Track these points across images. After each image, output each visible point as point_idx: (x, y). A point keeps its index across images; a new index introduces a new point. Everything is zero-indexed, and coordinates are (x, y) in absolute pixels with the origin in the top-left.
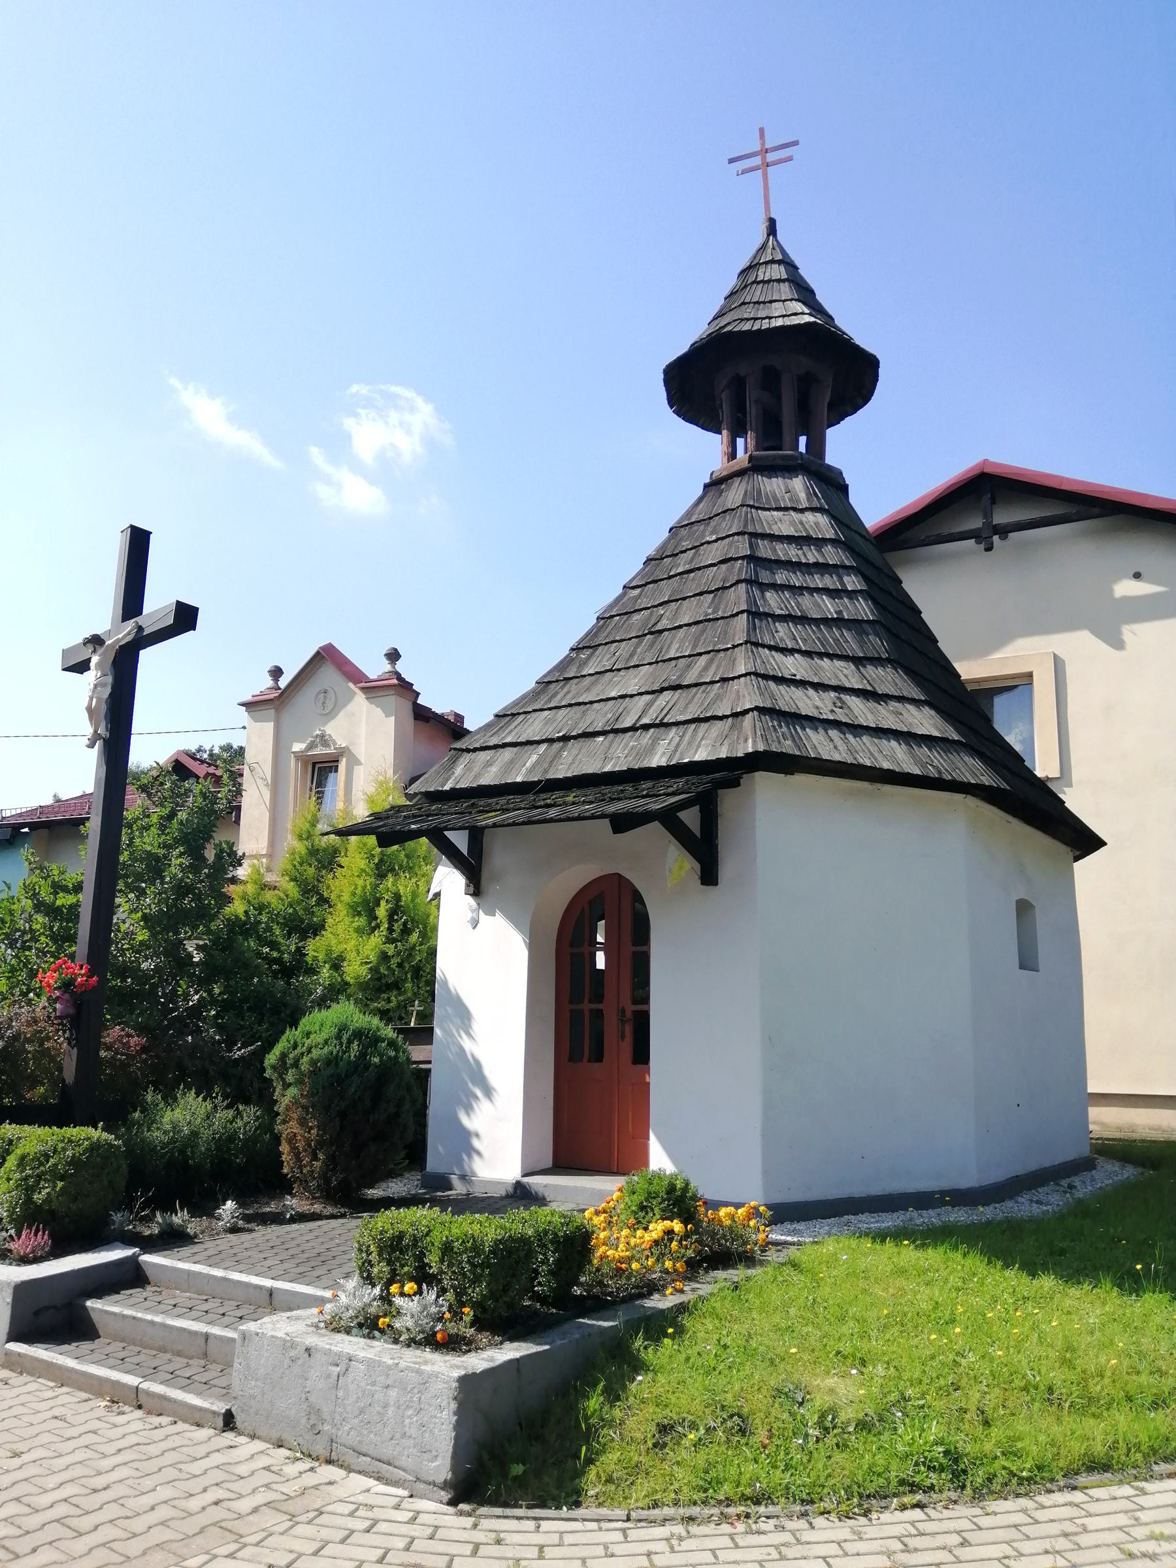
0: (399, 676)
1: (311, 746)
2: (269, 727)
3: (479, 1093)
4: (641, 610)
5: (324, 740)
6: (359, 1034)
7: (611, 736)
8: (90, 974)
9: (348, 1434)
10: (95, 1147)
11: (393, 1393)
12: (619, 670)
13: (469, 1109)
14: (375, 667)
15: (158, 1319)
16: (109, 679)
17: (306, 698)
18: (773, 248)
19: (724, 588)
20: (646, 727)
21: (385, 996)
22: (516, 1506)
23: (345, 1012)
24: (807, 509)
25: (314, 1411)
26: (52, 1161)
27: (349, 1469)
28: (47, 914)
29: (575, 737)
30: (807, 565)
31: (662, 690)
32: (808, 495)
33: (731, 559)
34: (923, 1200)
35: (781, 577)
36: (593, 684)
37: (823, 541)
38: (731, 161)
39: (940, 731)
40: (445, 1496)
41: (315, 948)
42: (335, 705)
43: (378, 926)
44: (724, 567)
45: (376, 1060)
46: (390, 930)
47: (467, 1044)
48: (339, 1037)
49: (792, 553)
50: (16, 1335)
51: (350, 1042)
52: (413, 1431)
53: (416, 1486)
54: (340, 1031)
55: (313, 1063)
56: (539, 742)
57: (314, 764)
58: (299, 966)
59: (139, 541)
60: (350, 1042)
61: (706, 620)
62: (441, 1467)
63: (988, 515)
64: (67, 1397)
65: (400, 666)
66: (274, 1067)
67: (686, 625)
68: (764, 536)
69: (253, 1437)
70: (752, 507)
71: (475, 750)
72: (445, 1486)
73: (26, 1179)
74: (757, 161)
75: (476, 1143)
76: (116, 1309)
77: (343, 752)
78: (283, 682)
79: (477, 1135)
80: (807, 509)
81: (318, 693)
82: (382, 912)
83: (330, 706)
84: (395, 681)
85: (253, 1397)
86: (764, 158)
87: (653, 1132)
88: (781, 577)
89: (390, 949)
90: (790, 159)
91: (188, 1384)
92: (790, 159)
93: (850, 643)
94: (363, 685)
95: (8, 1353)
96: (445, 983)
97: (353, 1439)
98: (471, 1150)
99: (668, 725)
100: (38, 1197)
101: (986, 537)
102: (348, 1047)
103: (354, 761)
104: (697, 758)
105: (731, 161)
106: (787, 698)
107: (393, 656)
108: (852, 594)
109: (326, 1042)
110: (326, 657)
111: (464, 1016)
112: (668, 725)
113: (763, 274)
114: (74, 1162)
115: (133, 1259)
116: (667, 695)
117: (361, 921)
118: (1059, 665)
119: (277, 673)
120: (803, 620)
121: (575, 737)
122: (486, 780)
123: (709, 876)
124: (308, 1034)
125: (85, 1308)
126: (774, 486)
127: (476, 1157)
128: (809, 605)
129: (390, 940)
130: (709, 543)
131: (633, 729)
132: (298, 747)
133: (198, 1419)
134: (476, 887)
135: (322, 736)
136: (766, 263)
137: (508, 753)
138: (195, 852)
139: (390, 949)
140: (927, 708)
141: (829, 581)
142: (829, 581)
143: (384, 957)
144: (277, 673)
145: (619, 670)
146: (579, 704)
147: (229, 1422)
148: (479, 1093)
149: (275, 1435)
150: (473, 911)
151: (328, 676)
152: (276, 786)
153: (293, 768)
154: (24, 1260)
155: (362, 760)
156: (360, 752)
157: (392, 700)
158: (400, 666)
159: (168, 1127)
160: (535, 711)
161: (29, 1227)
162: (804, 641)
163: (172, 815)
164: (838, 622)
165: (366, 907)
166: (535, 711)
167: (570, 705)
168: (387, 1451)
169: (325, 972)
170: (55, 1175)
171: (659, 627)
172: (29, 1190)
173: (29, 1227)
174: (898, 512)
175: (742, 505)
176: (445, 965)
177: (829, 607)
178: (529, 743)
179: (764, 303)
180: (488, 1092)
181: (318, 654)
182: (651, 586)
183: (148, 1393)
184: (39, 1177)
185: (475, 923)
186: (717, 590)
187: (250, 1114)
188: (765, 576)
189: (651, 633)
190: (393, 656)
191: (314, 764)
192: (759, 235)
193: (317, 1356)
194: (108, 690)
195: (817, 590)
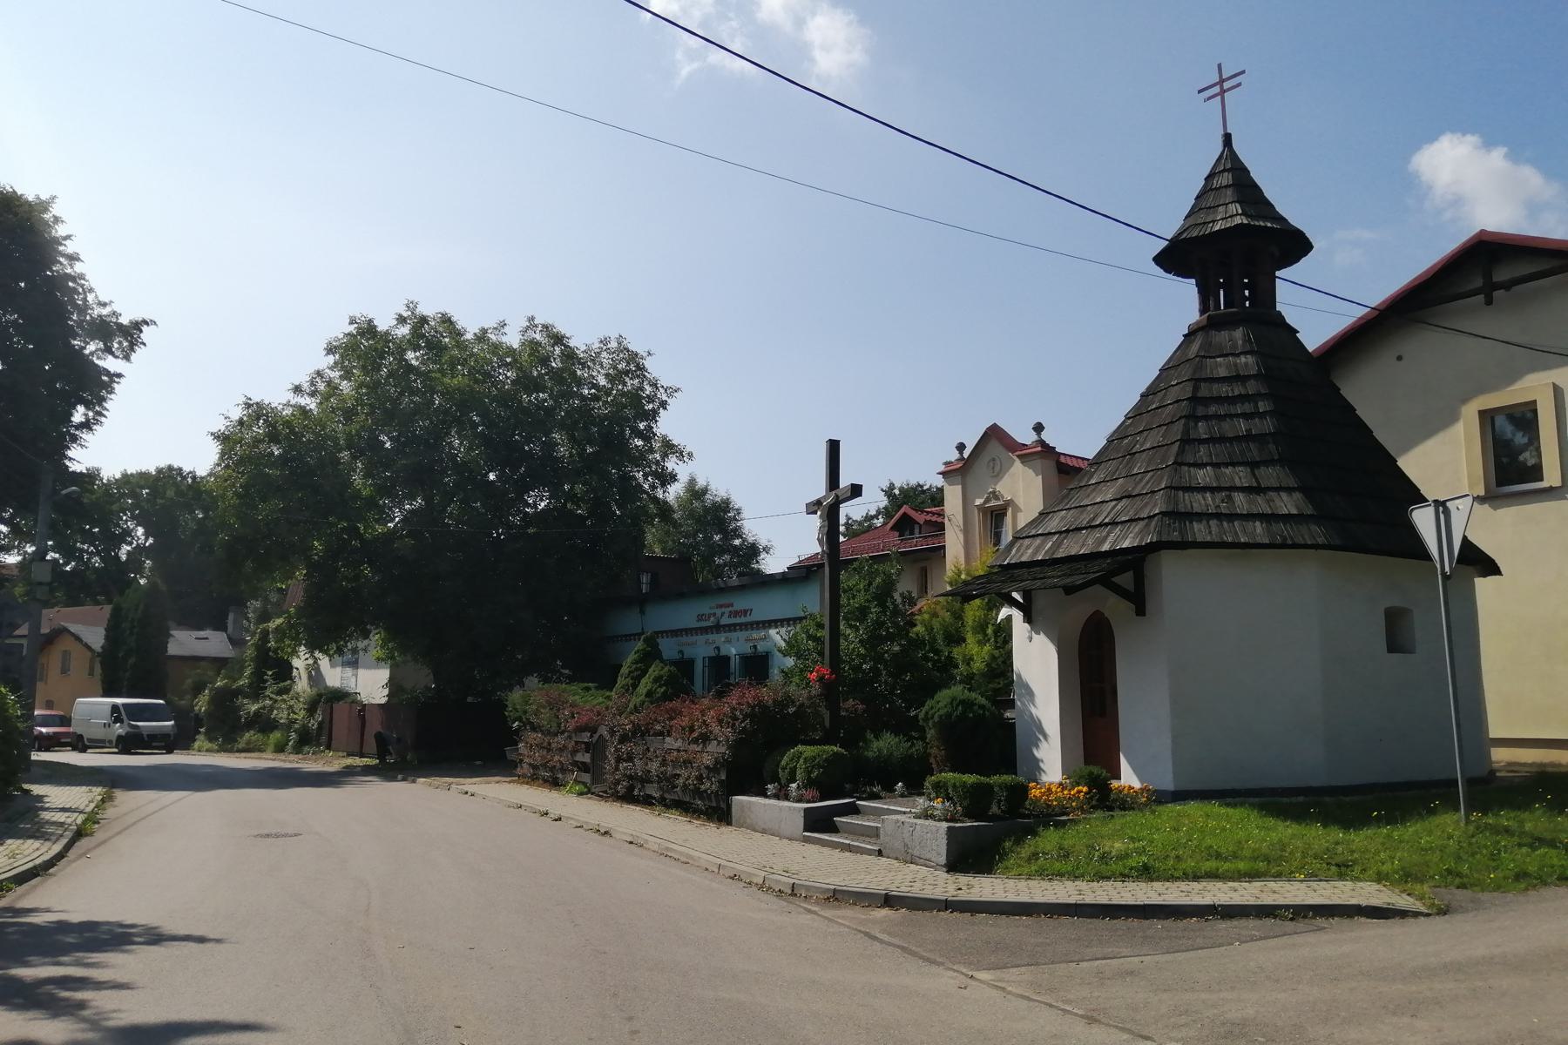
0: (1042, 443)
1: (987, 500)
2: (959, 488)
3: (1041, 738)
4: (1128, 436)
5: (995, 495)
6: (962, 702)
7: (1089, 530)
8: (831, 673)
9: (916, 853)
10: (835, 754)
11: (929, 835)
12: (1108, 481)
13: (1037, 747)
14: (1026, 437)
15: (860, 823)
16: (826, 523)
17: (981, 467)
18: (1226, 158)
19: (1172, 422)
20: (1107, 525)
21: (997, 681)
22: (969, 873)
23: (957, 691)
24: (1241, 353)
25: (906, 845)
26: (817, 760)
27: (917, 865)
28: (814, 641)
29: (1072, 530)
30: (1234, 397)
31: (1121, 498)
32: (1244, 341)
33: (1180, 400)
34: (1274, 792)
35: (1213, 409)
36: (1094, 490)
37: (1248, 377)
38: (1200, 92)
39: (1298, 508)
40: (945, 869)
41: (957, 652)
42: (1001, 466)
43: (989, 640)
44: (1176, 405)
45: (971, 715)
46: (996, 642)
47: (1033, 710)
48: (951, 703)
49: (1224, 390)
50: (805, 830)
51: (958, 706)
52: (935, 848)
53: (936, 867)
54: (953, 700)
55: (940, 717)
56: (1055, 533)
57: (992, 512)
58: (951, 663)
59: (834, 447)
60: (958, 706)
61: (1159, 446)
62: (943, 860)
63: (1488, 276)
64: (826, 850)
65: (1045, 436)
66: (923, 719)
67: (1147, 449)
68: (1206, 380)
69: (888, 858)
70: (1204, 357)
71: (1023, 538)
72: (945, 866)
73: (807, 767)
74: (1217, 89)
75: (1041, 765)
76: (845, 820)
77: (1009, 503)
78: (966, 454)
79: (1042, 761)
80: (1241, 353)
81: (989, 462)
82: (990, 631)
83: (997, 468)
84: (1039, 449)
85: (887, 843)
86: (1222, 87)
87: (1125, 756)
88: (1213, 409)
89: (996, 653)
90: (1239, 85)
91: (869, 843)
92: (1239, 85)
93: (1254, 452)
94: (1017, 453)
95: (804, 836)
96: (1019, 676)
97: (917, 854)
98: (1040, 770)
99: (1117, 523)
100: (813, 775)
101: (1488, 292)
102: (956, 709)
103: (1017, 510)
104: (1124, 546)
105: (1200, 92)
106: (1187, 502)
107: (1039, 428)
108: (1262, 415)
109: (946, 706)
110: (994, 435)
111: (1030, 693)
112: (1117, 523)
113: (1216, 183)
114: (826, 760)
115: (854, 802)
116: (1124, 501)
117: (980, 637)
118: (1557, 391)
119: (961, 447)
120: (1222, 440)
121: (1072, 530)
122: (1024, 559)
123: (1141, 611)
124: (938, 702)
125: (834, 821)
126: (1222, 337)
127: (1043, 774)
128: (1227, 428)
129: (997, 648)
130: (1173, 386)
131: (1100, 525)
132: (979, 502)
133: (869, 852)
134: (1028, 619)
135: (994, 492)
136: (1220, 172)
137: (1038, 541)
138: (882, 604)
139: (996, 653)
140: (1297, 493)
141: (1247, 408)
142: (1247, 408)
143: (993, 658)
144: (961, 447)
145: (1108, 481)
146: (1080, 506)
147: (880, 853)
148: (1041, 738)
149: (895, 856)
150: (1029, 632)
151: (995, 448)
152: (966, 530)
153: (976, 518)
154: (809, 802)
155: (1022, 508)
156: (1020, 502)
157: (1038, 463)
158: (1045, 436)
159: (876, 750)
160: (1058, 511)
161: (810, 788)
162: (1216, 455)
163: (870, 584)
164: (1249, 437)
165: (981, 628)
166: (1058, 511)
167: (1076, 507)
168: (928, 856)
169: (962, 668)
170: (819, 766)
171: (1134, 451)
172: (810, 773)
173: (810, 788)
174: (1415, 279)
175: (1196, 356)
176: (1018, 663)
177: (1242, 426)
178: (1050, 534)
179: (1214, 207)
180: (1045, 736)
181: (985, 433)
182: (1138, 417)
183: (853, 845)
184: (813, 767)
185: (1031, 639)
186: (1168, 423)
187: (919, 745)
188: (1200, 411)
189: (1129, 454)
190: (1039, 428)
191: (992, 512)
192: (1217, 148)
193: (906, 824)
194: (826, 529)
195: (1237, 416)
